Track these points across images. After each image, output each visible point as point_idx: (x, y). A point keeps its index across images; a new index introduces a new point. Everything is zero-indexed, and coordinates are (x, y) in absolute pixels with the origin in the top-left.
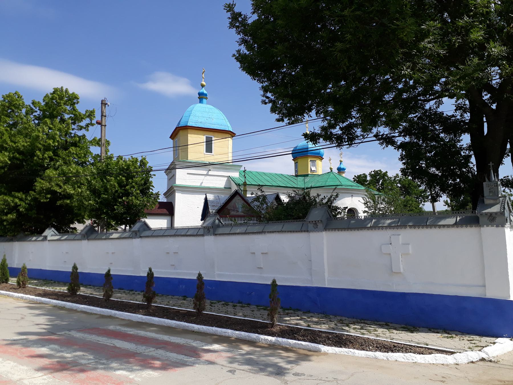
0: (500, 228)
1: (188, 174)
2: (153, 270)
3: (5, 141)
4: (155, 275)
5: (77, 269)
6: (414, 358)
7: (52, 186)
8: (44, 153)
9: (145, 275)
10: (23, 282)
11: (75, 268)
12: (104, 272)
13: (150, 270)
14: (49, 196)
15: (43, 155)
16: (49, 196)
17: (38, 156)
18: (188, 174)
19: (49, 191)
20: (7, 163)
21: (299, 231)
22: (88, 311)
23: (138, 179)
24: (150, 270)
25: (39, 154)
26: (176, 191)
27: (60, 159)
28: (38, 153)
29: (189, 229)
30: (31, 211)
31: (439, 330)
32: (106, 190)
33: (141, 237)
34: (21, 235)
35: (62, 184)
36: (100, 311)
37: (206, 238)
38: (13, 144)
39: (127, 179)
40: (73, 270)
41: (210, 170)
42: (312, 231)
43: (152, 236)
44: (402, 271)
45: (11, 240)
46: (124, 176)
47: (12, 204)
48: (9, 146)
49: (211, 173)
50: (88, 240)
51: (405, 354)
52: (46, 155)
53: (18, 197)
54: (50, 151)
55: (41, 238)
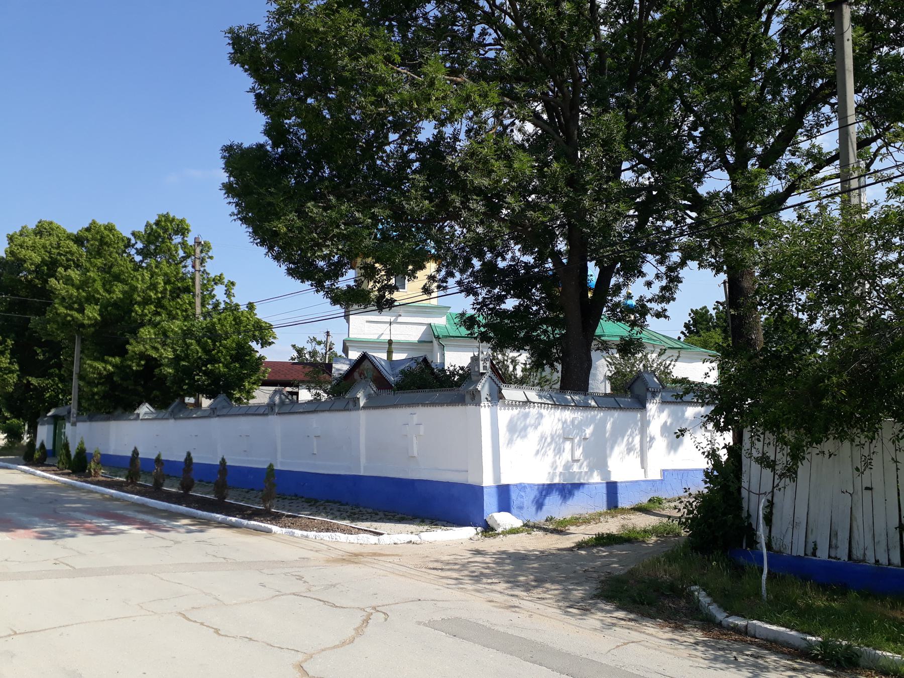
0: (471, 408)
1: (367, 322)
2: (192, 455)
3: (97, 292)
4: (195, 461)
5: (138, 454)
6: (338, 538)
7: (147, 350)
8: (144, 308)
9: (182, 460)
10: (94, 470)
11: (189, 457)
12: (154, 457)
13: (189, 454)
14: (143, 362)
15: (142, 311)
16: (143, 362)
17: (136, 312)
18: (367, 322)
19: (142, 356)
20: (96, 319)
21: (342, 410)
22: (780, 639)
23: (228, 342)
24: (189, 454)
25: (137, 309)
26: (350, 348)
27: (164, 312)
28: (137, 308)
29: (259, 406)
30: (815, 323)
31: (437, 522)
32: (187, 356)
33: (218, 416)
34: (119, 411)
35: (159, 346)
36: (137, 499)
37: (270, 417)
38: (107, 295)
39: (214, 342)
40: (133, 455)
41: (400, 315)
42: (353, 410)
43: (246, 414)
44: (416, 454)
45: (108, 419)
46: (210, 338)
47: (105, 373)
48: (102, 295)
49: (400, 319)
50: (175, 419)
51: (333, 534)
52: (146, 311)
53: (110, 363)
54: (151, 304)
55: (132, 417)
